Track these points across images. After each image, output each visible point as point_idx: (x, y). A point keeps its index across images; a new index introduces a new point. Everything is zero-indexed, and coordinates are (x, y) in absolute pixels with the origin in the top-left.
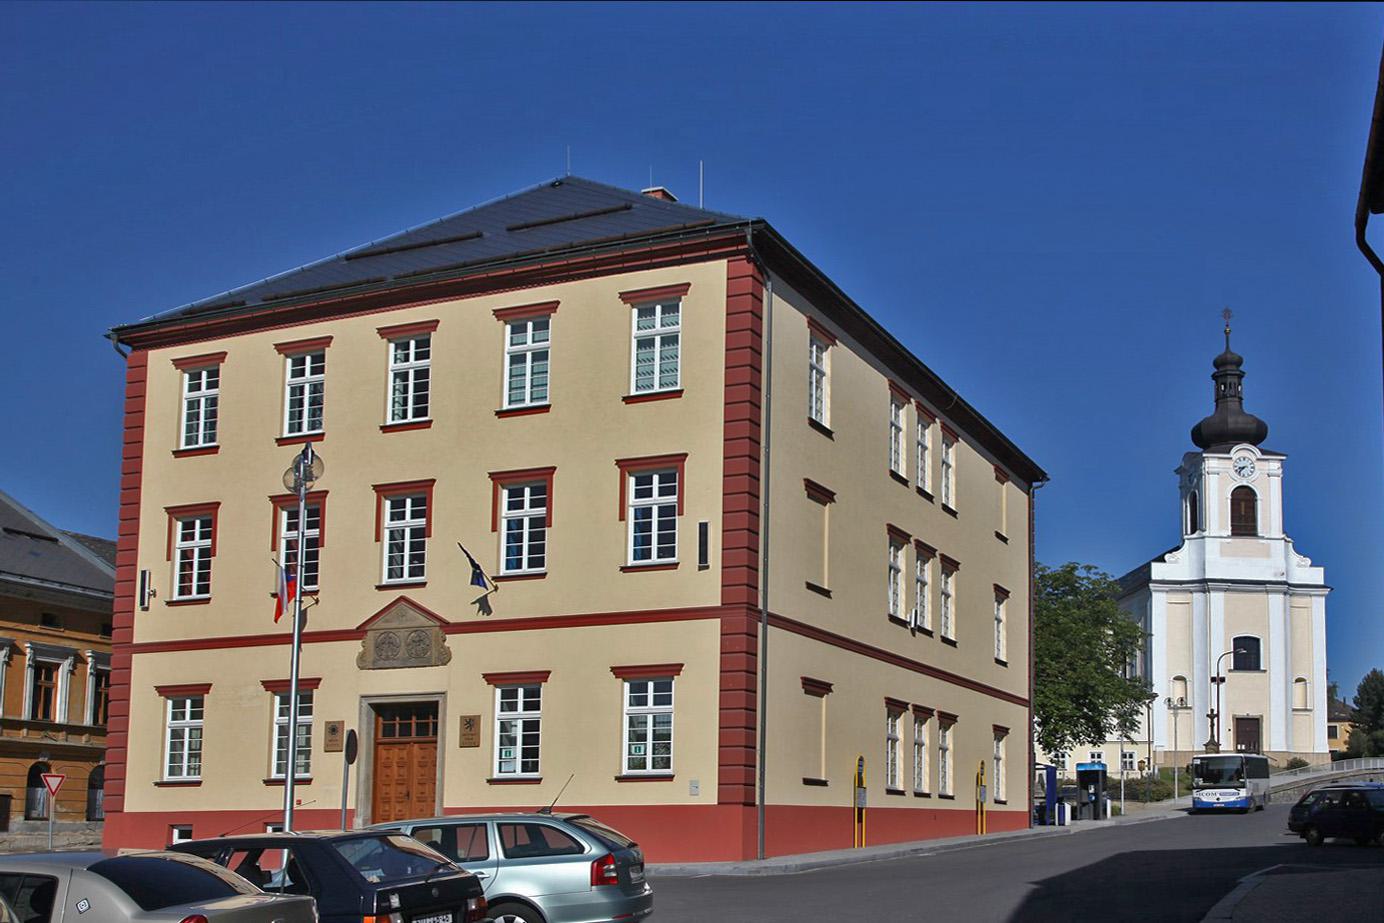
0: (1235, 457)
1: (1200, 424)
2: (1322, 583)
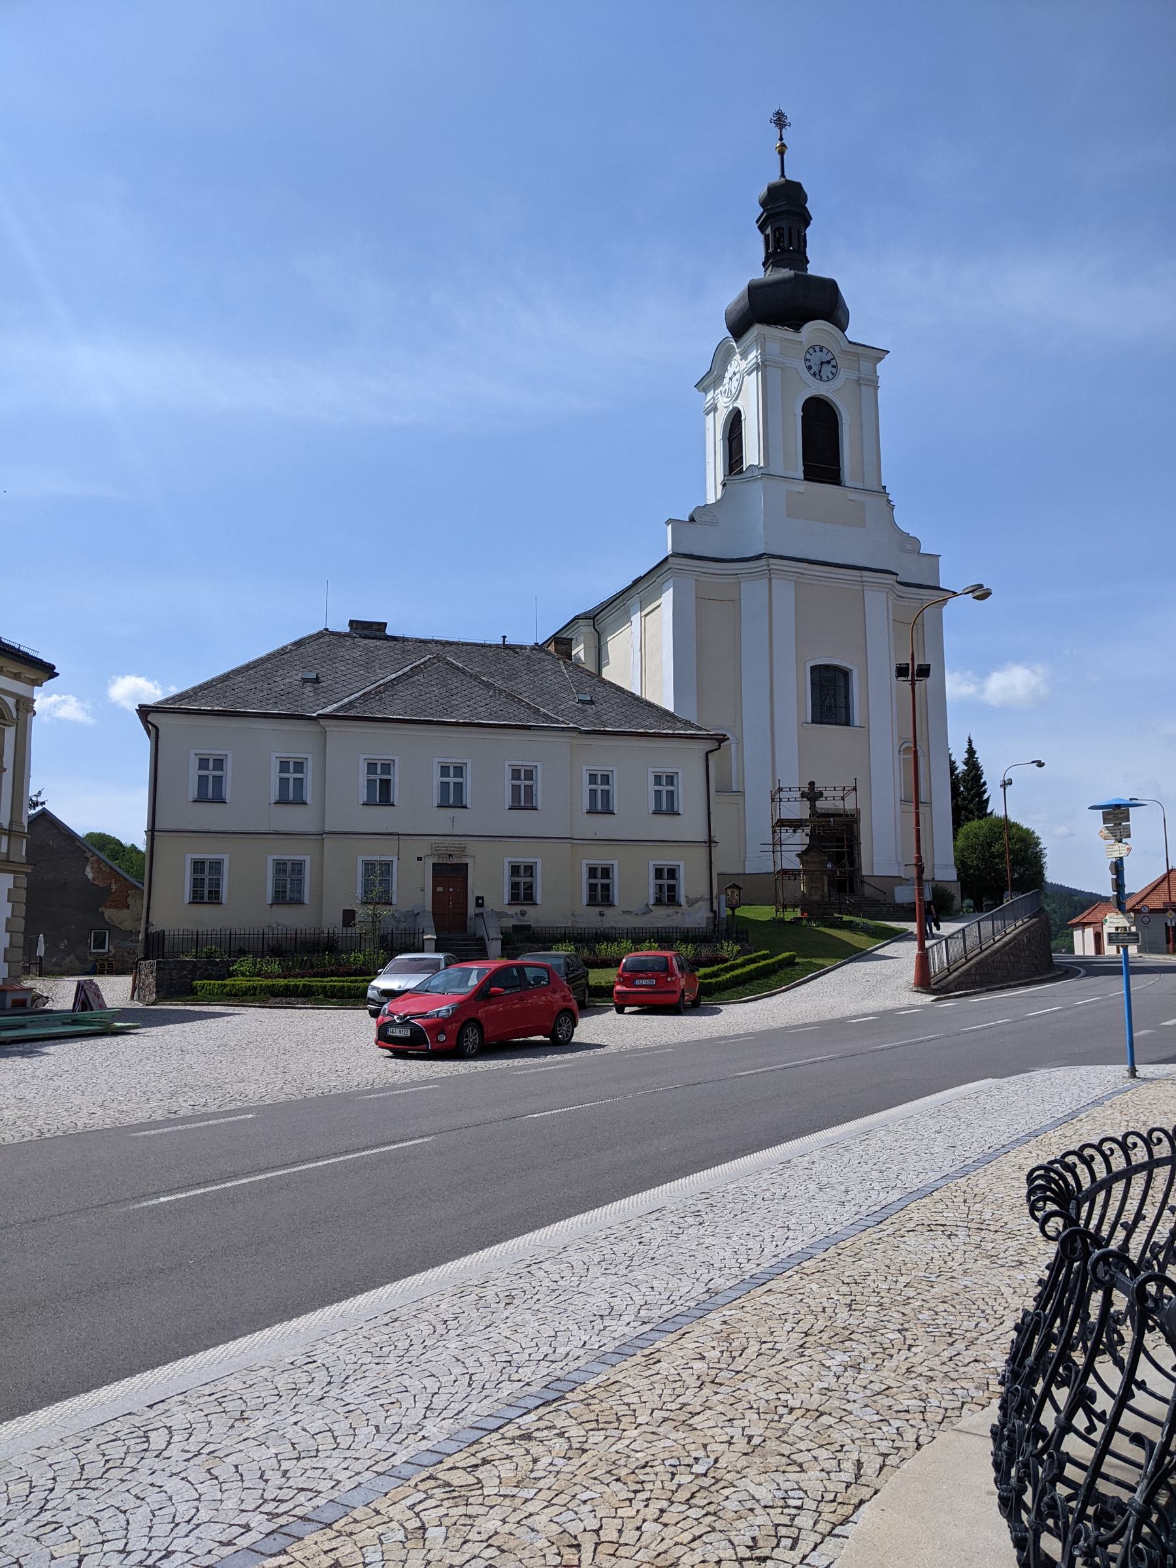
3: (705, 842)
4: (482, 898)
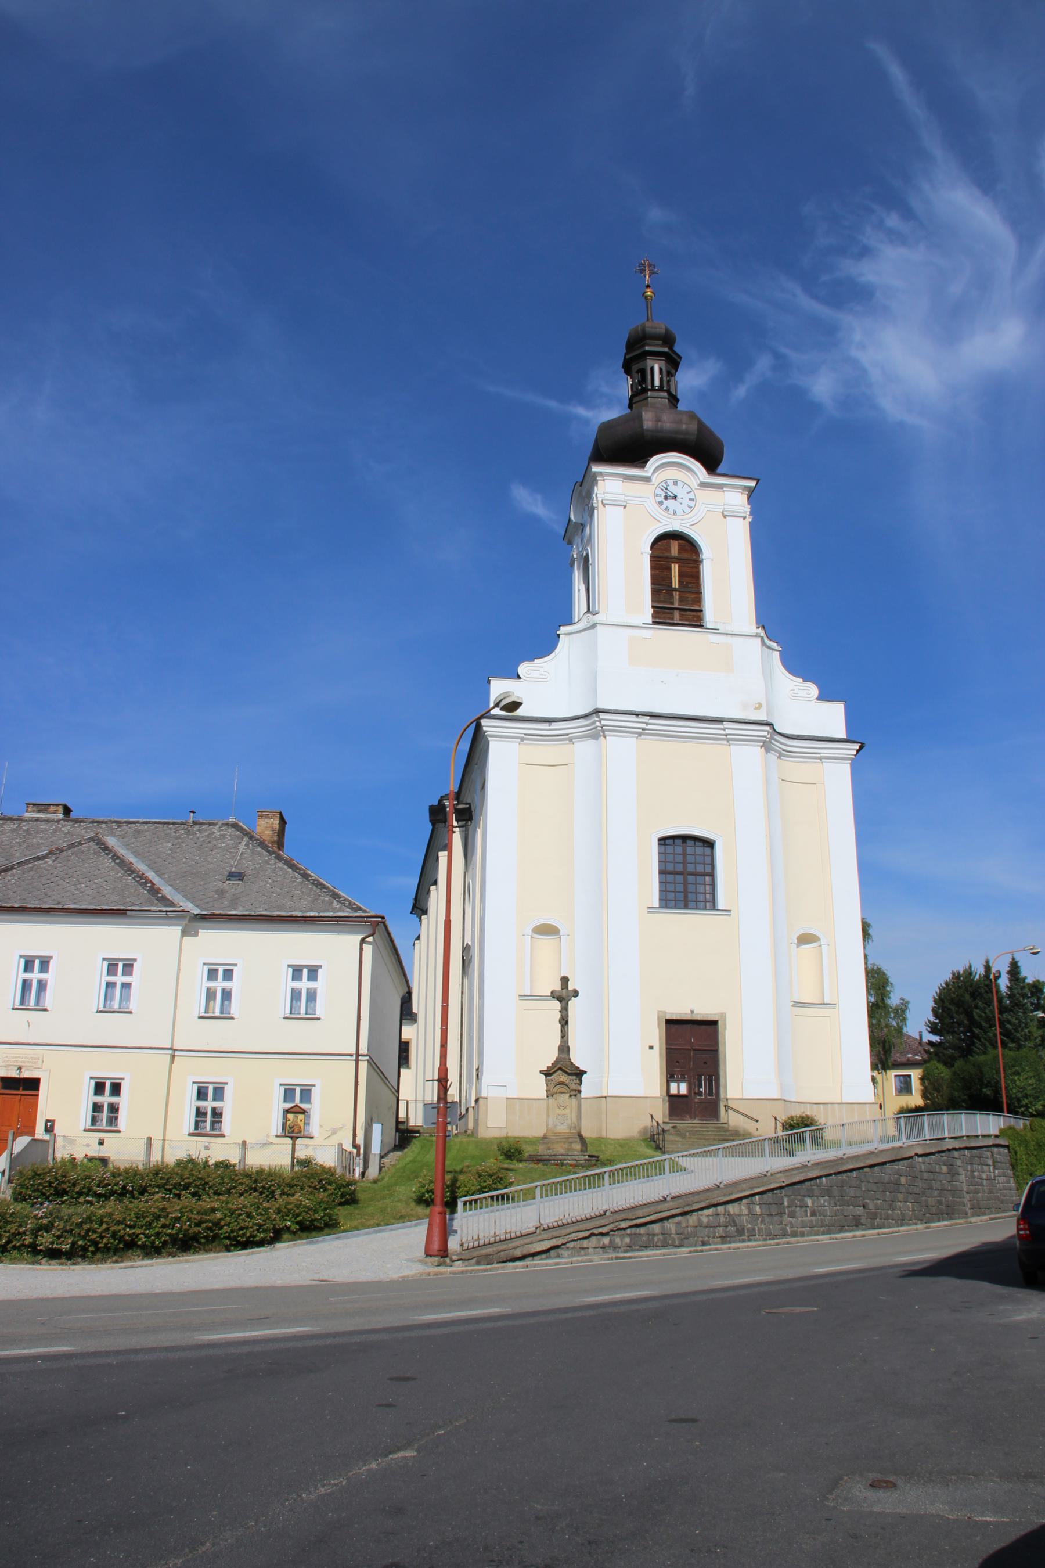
0: (657, 479)
1: (596, 440)
2: (844, 736)
3: (351, 1055)
4: (53, 1121)
